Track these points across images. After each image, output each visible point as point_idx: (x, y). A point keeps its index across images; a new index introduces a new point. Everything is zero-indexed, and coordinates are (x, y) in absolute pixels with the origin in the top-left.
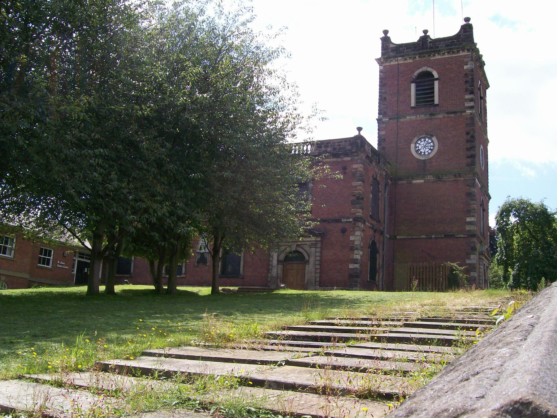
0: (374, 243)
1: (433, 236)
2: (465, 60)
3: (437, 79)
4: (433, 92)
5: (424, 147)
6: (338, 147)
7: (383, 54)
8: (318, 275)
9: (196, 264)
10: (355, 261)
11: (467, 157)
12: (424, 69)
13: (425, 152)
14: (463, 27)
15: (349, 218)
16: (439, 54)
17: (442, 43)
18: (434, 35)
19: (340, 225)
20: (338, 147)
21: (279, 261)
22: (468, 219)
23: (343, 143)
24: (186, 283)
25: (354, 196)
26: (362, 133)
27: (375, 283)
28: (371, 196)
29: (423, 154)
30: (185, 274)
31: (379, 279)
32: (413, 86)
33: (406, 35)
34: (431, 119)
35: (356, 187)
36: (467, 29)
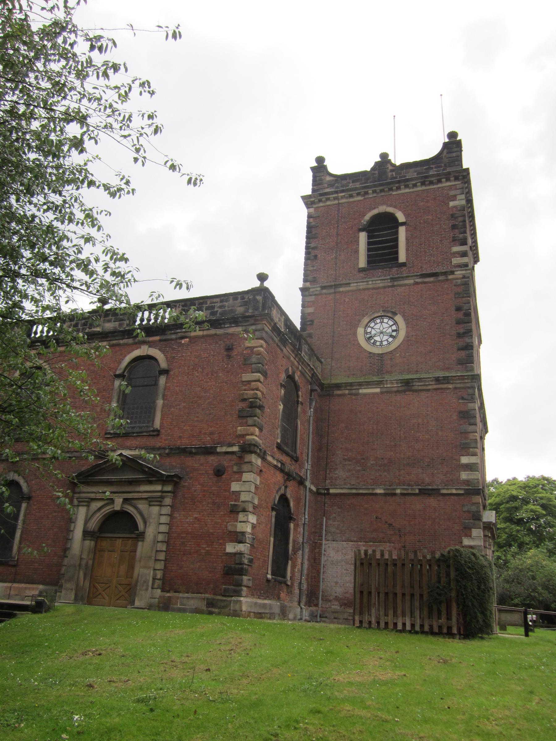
0: (284, 499)
1: (398, 491)
2: (452, 193)
3: (403, 224)
4: (397, 246)
5: (382, 334)
6: (220, 310)
7: (314, 191)
8: (160, 566)
10: (239, 538)
11: (459, 349)
12: (382, 209)
13: (381, 342)
16: (407, 186)
17: (412, 170)
18: (399, 158)
19: (212, 459)
20: (220, 310)
21: (86, 534)
22: (465, 460)
23: (231, 302)
25: (244, 400)
26: (266, 284)
27: (285, 583)
28: (281, 407)
29: (378, 344)
31: (293, 572)
32: (363, 237)
33: (352, 159)
34: (393, 286)
35: (249, 382)
36: (453, 145)
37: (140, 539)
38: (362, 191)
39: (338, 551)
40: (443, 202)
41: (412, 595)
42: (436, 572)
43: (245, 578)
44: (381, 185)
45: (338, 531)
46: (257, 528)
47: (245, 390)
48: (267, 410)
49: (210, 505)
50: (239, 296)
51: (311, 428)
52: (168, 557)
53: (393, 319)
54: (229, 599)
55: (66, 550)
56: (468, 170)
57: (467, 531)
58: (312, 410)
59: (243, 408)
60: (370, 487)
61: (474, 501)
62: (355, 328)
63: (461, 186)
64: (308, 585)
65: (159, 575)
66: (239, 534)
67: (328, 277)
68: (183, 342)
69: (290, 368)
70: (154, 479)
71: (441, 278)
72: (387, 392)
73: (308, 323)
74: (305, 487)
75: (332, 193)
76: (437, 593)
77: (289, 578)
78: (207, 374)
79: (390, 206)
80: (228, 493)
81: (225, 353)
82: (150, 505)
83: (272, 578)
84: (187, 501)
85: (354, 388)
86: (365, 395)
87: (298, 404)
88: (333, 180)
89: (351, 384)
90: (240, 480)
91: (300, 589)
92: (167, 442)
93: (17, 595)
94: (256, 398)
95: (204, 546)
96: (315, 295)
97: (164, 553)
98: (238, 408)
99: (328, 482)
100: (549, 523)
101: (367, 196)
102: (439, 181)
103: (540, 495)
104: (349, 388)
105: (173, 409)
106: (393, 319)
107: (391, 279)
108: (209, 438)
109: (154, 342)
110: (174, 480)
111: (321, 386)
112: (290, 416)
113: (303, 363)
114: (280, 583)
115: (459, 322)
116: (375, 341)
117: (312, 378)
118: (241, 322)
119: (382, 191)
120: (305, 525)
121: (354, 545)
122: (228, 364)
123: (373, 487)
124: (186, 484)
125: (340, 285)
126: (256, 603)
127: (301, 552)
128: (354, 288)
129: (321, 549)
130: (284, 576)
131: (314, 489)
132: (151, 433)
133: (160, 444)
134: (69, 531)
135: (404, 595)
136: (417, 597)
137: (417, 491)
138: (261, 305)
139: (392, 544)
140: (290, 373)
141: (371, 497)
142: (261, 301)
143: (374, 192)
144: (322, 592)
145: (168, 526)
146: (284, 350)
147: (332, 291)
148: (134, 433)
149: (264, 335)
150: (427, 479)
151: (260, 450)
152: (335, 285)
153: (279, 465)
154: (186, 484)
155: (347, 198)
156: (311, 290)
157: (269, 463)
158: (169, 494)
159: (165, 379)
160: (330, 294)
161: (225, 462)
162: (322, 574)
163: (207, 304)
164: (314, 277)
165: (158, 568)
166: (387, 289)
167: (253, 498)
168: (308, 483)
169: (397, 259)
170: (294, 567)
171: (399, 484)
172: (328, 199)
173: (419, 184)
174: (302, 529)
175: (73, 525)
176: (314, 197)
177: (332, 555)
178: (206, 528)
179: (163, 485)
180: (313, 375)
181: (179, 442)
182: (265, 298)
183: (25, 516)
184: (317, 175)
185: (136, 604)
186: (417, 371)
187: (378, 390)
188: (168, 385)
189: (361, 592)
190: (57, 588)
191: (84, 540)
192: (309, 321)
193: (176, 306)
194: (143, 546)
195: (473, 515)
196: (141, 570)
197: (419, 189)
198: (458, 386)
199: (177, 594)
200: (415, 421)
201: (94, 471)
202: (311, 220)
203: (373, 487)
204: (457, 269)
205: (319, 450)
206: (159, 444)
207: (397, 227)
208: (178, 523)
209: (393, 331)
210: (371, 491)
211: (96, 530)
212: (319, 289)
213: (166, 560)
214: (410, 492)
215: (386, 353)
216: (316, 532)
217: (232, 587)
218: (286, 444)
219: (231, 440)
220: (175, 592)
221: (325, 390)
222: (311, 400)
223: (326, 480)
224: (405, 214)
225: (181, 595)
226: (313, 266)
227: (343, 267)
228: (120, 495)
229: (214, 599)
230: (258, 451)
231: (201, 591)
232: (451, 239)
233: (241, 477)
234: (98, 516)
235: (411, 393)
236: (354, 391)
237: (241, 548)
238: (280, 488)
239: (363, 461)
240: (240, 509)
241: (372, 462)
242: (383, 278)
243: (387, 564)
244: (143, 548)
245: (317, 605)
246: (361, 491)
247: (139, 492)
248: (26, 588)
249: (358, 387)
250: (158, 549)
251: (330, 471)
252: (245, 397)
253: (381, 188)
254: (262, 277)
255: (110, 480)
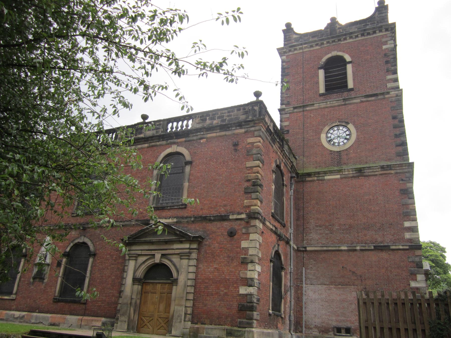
0: (277, 254)
1: (358, 248)
2: (384, 40)
3: (350, 62)
4: (346, 77)
5: (339, 137)
7: (285, 45)
8: (190, 304)
9: (31, 280)
10: (249, 282)
11: (397, 146)
12: (334, 53)
13: (339, 143)
14: (377, 9)
15: (242, 213)
16: (351, 38)
17: (354, 27)
18: (343, 21)
19: (225, 224)
20: (228, 118)
21: (135, 280)
22: (407, 224)
24: (14, 307)
25: (248, 181)
26: (260, 99)
28: (273, 187)
29: (337, 144)
30: (16, 294)
32: (321, 73)
33: (310, 23)
34: (345, 105)
35: (251, 168)
36: (382, 9)
37: (174, 284)
38: (319, 43)
39: (315, 292)
40: (378, 46)
41: (415, 330)
42: (435, 310)
43: (255, 313)
44: (332, 38)
45: (314, 277)
46: (262, 275)
47: (249, 173)
48: (265, 188)
49: (226, 259)
50: (242, 108)
51: (292, 203)
52: (195, 298)
53: (346, 127)
54: (244, 329)
55: (120, 292)
56: (387, 6)
57: (413, 276)
58: (292, 191)
59: (248, 186)
60: (336, 245)
61: (416, 254)
62: (319, 134)
63: (390, 35)
64: (294, 317)
65: (189, 311)
66: (249, 280)
67: (298, 101)
68: (202, 141)
69: (278, 160)
70: (184, 239)
71: (380, 97)
72: (345, 178)
73: (285, 132)
74: (290, 246)
75: (298, 45)
76: (439, 329)
77: (283, 313)
78: (220, 163)
79: (340, 51)
80: (239, 249)
81: (233, 148)
82: (181, 259)
83: (273, 313)
84: (208, 255)
85: (321, 175)
86: (329, 180)
87: (283, 186)
88: (298, 37)
89: (319, 173)
90: (248, 239)
91: (290, 321)
92: (192, 213)
93: (86, 325)
94: (258, 179)
95: (222, 289)
96: (289, 113)
97: (192, 295)
98: (244, 186)
99: (305, 242)
100: (437, 272)
101: (322, 46)
102: (374, 32)
103: (430, 253)
104: (317, 176)
105: (196, 189)
106: (346, 127)
107: (344, 99)
108: (223, 209)
109: (181, 142)
110: (199, 240)
111: (297, 174)
112: (279, 194)
113: (286, 157)
114: (278, 316)
115: (395, 127)
116: (334, 143)
117: (291, 169)
118: (244, 125)
119: (334, 41)
120: (292, 274)
121: (327, 287)
122: (235, 156)
123: (339, 245)
124: (207, 243)
125: (307, 106)
126: (263, 332)
127: (289, 293)
128: (317, 107)
129: (302, 290)
130: (280, 311)
131: (296, 247)
132: (181, 207)
133: (187, 214)
134: (123, 278)
135: (406, 330)
136: (419, 332)
137: (373, 248)
138: (258, 113)
139: (356, 287)
140: (278, 164)
141: (337, 253)
142: (258, 110)
143: (328, 42)
144: (305, 322)
145: (195, 274)
146: (274, 146)
147: (301, 110)
148: (168, 207)
149: (261, 134)
150: (379, 239)
151: (262, 217)
152: (303, 106)
153: (274, 229)
154: (207, 243)
155: (309, 48)
156: (286, 110)
157: (267, 227)
158: (195, 251)
159: (189, 168)
160: (300, 112)
161: (236, 225)
162: (304, 309)
163: (218, 114)
164: (288, 102)
165: (189, 306)
166: (341, 107)
167: (258, 252)
168: (291, 243)
169: (347, 86)
170: (285, 304)
171: (358, 243)
172: (295, 50)
173: (359, 35)
174: (289, 276)
175: (125, 274)
176: (286, 49)
177: (310, 295)
178: (223, 275)
179: (190, 244)
180: (292, 166)
181: (201, 212)
182: (260, 108)
183: (92, 267)
184: (287, 34)
185: (172, 333)
186: (366, 162)
187: (338, 176)
188: (192, 172)
189: (367, 328)
190: (115, 320)
191: (133, 285)
192: (285, 131)
193: (196, 117)
194: (176, 289)
195: (417, 265)
196: (176, 307)
197: (360, 39)
198: (398, 171)
199: (203, 326)
200: (367, 197)
201: (140, 234)
202: (284, 64)
203: (339, 245)
204: (390, 91)
205: (297, 220)
206: (186, 215)
207: (345, 65)
208: (203, 272)
209: (347, 135)
210: (337, 248)
211: (142, 277)
212: (292, 109)
213: (194, 300)
214: (367, 248)
215: (343, 151)
216: (298, 279)
217: (245, 320)
218: (277, 215)
219: (239, 210)
220: (202, 324)
221: (300, 178)
222: (291, 184)
223: (303, 241)
224: (350, 56)
225: (206, 326)
226: (287, 94)
227: (308, 94)
228: (159, 251)
229: (232, 330)
230: (260, 218)
231: (222, 323)
232: (386, 71)
233: (249, 237)
234: (144, 267)
235: (363, 177)
236: (321, 178)
237: (251, 290)
238: (275, 246)
239: (330, 227)
240: (249, 261)
241: (337, 228)
242: (337, 99)
243: (388, 304)
244: (177, 291)
245: (301, 332)
246: (330, 248)
247: (173, 249)
248: (92, 320)
249: (323, 175)
250: (188, 292)
251: (306, 235)
252: (249, 178)
253: (333, 39)
254: (257, 94)
255: (151, 241)
